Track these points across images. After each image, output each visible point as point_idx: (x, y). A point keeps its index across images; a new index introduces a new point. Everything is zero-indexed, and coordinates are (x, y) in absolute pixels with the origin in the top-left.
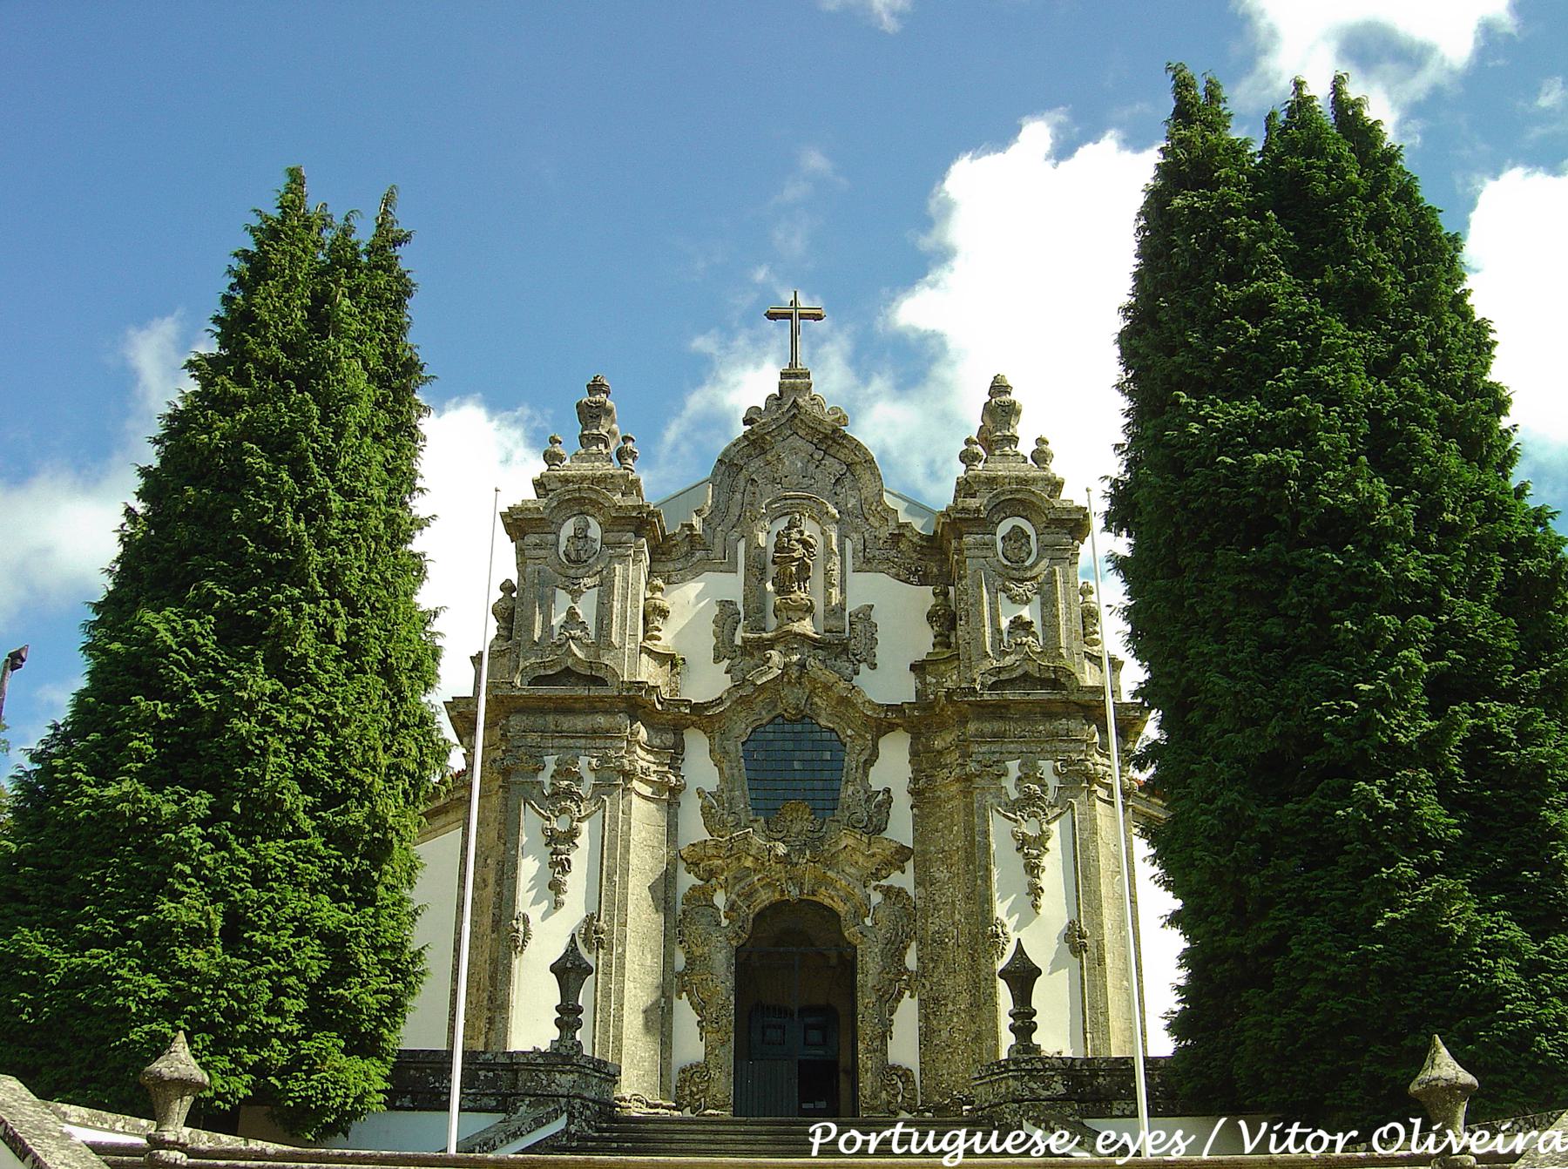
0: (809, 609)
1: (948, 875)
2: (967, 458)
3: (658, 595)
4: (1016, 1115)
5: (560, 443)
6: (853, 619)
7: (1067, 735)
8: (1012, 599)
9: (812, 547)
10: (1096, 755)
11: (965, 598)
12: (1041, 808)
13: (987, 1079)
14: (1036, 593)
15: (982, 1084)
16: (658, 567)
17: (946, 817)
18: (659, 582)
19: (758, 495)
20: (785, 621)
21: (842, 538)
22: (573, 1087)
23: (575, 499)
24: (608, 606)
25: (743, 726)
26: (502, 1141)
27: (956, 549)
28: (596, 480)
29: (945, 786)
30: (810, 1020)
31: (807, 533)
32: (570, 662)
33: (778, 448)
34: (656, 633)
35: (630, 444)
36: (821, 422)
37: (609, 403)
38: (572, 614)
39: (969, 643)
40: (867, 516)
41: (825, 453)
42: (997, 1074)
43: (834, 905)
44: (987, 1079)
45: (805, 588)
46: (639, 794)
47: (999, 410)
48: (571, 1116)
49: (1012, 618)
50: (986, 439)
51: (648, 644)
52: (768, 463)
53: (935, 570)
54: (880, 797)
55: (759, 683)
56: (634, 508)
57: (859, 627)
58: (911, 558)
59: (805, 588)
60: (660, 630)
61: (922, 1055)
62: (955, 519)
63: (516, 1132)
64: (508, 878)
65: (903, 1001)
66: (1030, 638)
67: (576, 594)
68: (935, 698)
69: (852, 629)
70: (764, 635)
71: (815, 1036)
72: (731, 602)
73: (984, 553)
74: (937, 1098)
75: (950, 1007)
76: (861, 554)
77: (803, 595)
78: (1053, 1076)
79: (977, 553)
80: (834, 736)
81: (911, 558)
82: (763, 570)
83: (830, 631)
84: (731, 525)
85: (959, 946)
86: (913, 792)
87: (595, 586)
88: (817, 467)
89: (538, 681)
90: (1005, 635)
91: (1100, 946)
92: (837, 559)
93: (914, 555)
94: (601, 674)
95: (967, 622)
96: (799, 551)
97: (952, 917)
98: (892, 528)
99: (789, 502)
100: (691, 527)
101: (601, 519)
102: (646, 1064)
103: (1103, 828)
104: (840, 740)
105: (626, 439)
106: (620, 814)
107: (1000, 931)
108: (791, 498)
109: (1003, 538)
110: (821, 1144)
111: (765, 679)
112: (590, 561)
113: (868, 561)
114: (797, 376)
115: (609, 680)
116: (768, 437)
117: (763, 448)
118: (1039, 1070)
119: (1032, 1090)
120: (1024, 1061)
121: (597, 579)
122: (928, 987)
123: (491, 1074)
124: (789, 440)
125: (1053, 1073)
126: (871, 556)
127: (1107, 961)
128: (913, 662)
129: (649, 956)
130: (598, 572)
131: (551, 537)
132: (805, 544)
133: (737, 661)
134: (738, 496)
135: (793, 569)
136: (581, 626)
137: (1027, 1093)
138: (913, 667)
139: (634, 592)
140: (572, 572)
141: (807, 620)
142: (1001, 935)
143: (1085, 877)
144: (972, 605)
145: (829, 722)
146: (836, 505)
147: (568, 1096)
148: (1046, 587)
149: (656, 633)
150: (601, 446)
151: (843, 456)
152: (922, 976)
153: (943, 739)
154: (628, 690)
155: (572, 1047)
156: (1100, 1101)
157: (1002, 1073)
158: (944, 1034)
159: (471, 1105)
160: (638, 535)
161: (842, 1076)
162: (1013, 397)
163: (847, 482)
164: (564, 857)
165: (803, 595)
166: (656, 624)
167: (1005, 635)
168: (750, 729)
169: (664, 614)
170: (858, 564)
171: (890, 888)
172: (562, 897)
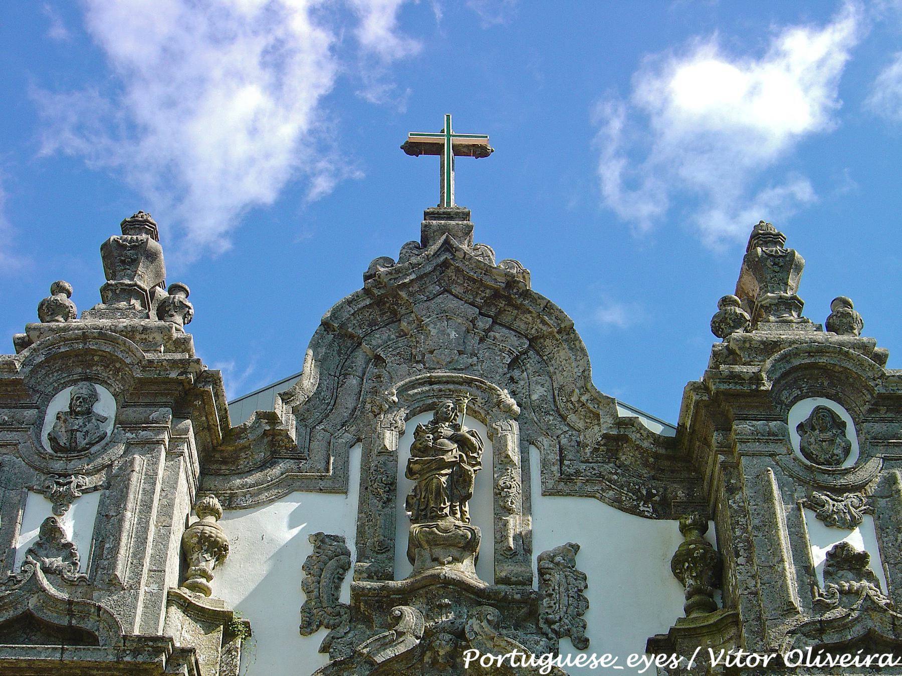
0: (469, 546)
3: (211, 519)
6: (546, 564)
8: (827, 520)
9: (473, 449)
11: (742, 521)
14: (865, 512)
16: (213, 482)
18: (215, 502)
19: (385, 379)
20: (429, 562)
21: (526, 442)
23: (77, 354)
24: (114, 520)
27: (721, 445)
31: (465, 429)
32: (32, 603)
33: (419, 309)
35: (181, 296)
38: (50, 531)
39: (756, 594)
41: (494, 322)
45: (462, 512)
47: (769, 263)
49: (829, 548)
52: (402, 334)
53: (680, 493)
55: (379, 659)
57: (556, 577)
58: (640, 476)
59: (462, 512)
62: (718, 393)
66: (864, 583)
67: (61, 502)
69: (544, 582)
70: (391, 583)
72: (335, 538)
73: (771, 448)
76: (555, 468)
79: (756, 447)
81: (640, 476)
82: (391, 486)
83: (506, 581)
84: (338, 421)
87: (96, 489)
88: (482, 340)
90: (820, 578)
92: (517, 473)
93: (644, 472)
94: (88, 625)
95: (749, 560)
96: (453, 453)
98: (606, 425)
99: (436, 387)
100: (272, 418)
101: (118, 387)
108: (439, 381)
109: (800, 427)
110: (470, 661)
111: (389, 653)
112: (93, 449)
113: (567, 478)
114: (449, 216)
115: (101, 635)
116: (403, 294)
117: (394, 313)
121: (99, 479)
124: (438, 300)
126: (572, 471)
128: (652, 636)
130: (104, 467)
131: (30, 413)
133: (341, 631)
134: (353, 381)
135: (443, 479)
136: (65, 553)
140: (58, 466)
141: (465, 562)
144: (756, 528)
146: (513, 394)
148: (882, 502)
151: (523, 326)
154: (136, 652)
160: (179, 415)
162: (788, 246)
163: (532, 361)
166: (203, 564)
167: (820, 578)
169: (218, 550)
170: (550, 484)
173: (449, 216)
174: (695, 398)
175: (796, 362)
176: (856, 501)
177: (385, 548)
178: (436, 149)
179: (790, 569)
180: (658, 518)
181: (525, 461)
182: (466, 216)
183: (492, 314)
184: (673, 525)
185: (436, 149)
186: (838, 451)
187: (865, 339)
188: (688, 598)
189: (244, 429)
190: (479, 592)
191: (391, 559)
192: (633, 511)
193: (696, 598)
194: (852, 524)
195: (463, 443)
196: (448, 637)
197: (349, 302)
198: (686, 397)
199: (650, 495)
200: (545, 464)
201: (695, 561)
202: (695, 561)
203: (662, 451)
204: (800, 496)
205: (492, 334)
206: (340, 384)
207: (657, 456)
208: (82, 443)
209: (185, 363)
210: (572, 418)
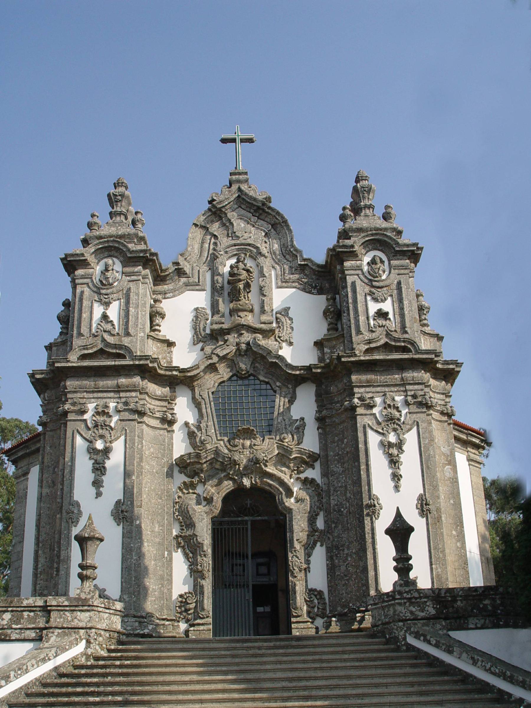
1: (342, 469)
2: (343, 218)
4: (401, 630)
5: (98, 217)
7: (413, 380)
8: (376, 300)
9: (251, 273)
10: (431, 393)
12: (399, 425)
13: (379, 605)
15: (376, 608)
17: (340, 434)
22: (89, 621)
25: (213, 382)
26: (33, 666)
28: (122, 237)
29: (338, 414)
30: (261, 560)
31: (248, 265)
34: (157, 327)
36: (255, 199)
37: (127, 193)
38: (105, 317)
40: (285, 255)
42: (387, 601)
43: (273, 491)
44: (379, 605)
45: (248, 297)
46: (148, 425)
48: (88, 642)
50: (354, 209)
51: (152, 334)
53: (327, 285)
54: (298, 423)
56: (141, 251)
59: (248, 297)
60: (160, 326)
61: (329, 582)
63: (45, 658)
64: (67, 480)
65: (316, 548)
67: (107, 304)
68: (330, 361)
71: (263, 570)
74: (339, 609)
75: (346, 551)
77: (247, 302)
78: (426, 602)
80: (268, 387)
85: (350, 513)
86: (318, 419)
89: (84, 357)
91: (438, 510)
97: (345, 495)
101: (122, 259)
102: (156, 593)
103: (437, 437)
104: (272, 389)
105: (136, 213)
106: (136, 438)
107: (376, 503)
114: (240, 174)
118: (416, 598)
119: (412, 613)
120: (406, 592)
122: (331, 539)
123: (32, 614)
125: (426, 600)
127: (443, 519)
128: (315, 340)
129: (157, 526)
132: (248, 271)
137: (408, 615)
138: (316, 344)
139: (143, 302)
140: (103, 291)
142: (377, 505)
143: (428, 467)
145: (266, 377)
147: (86, 628)
149: (157, 327)
150: (123, 218)
152: (328, 532)
153: (336, 386)
155: (89, 593)
156: (460, 618)
157: (390, 601)
158: (343, 568)
159: (18, 636)
161: (280, 594)
164: (101, 465)
165: (247, 302)
168: (217, 384)
171: (306, 479)
172: (101, 489)
173: (240, 174)
174: (331, 253)
176: (386, 292)
178: (234, 140)
180: (319, 294)
182: (246, 173)
183: (257, 215)
184: (324, 297)
185: (234, 140)
187: (395, 226)
188: (329, 325)
192: (310, 292)
193: (331, 326)
194: (384, 300)
195: (248, 271)
196: (245, 345)
198: (328, 253)
199: (316, 286)
200: (277, 276)
201: (331, 312)
202: (331, 312)
203: (320, 270)
204: (367, 289)
205: (257, 223)
209: (145, 251)
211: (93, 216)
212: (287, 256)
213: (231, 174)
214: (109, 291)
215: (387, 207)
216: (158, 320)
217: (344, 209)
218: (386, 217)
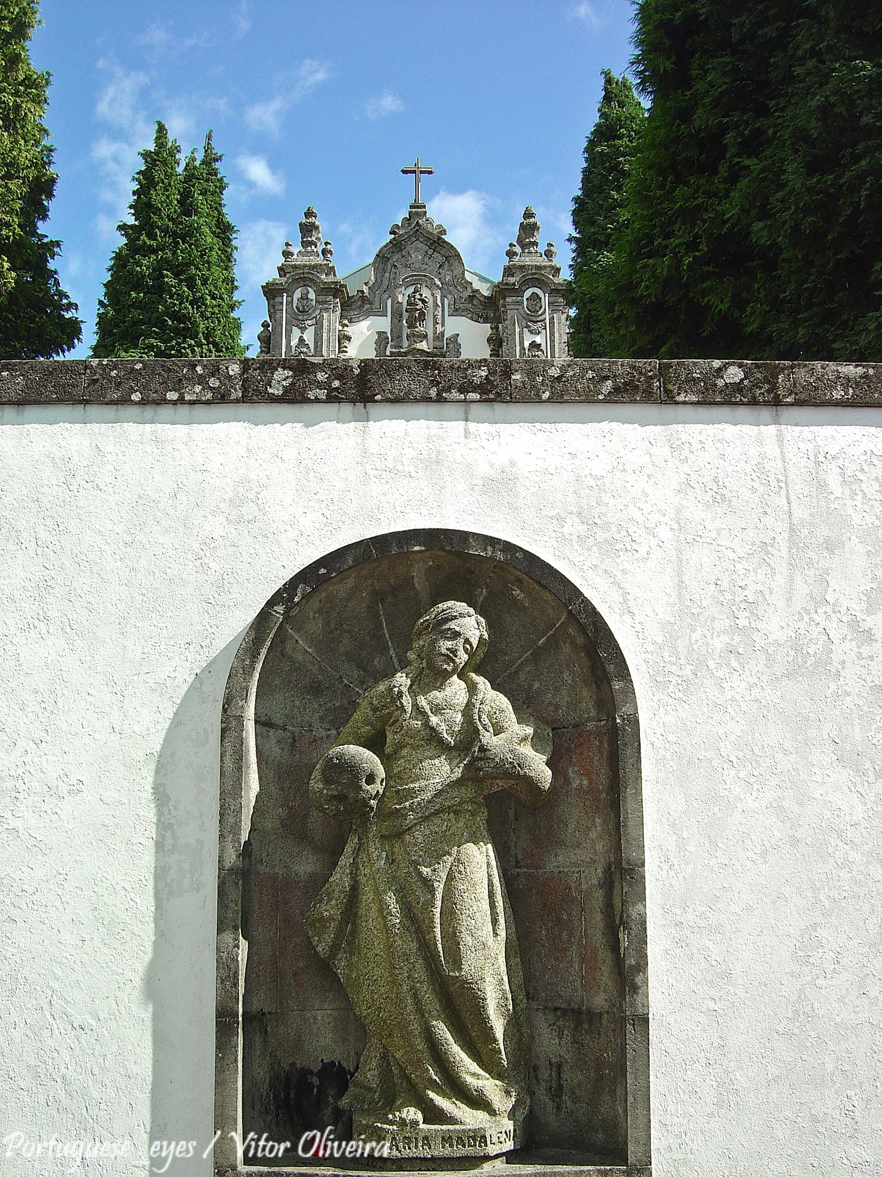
0: (425, 336)
6: (448, 341)
8: (531, 332)
9: (427, 303)
31: (424, 295)
34: (345, 349)
35: (329, 246)
38: (301, 340)
49: (530, 342)
57: (451, 346)
67: (303, 329)
69: (447, 347)
72: (384, 332)
73: (517, 307)
77: (422, 329)
79: (514, 307)
82: (401, 315)
92: (440, 309)
93: (481, 307)
98: (469, 292)
100: (362, 292)
105: (327, 243)
109: (527, 299)
113: (456, 310)
114: (418, 207)
121: (314, 321)
132: (423, 301)
140: (301, 318)
149: (345, 349)
160: (335, 298)
165: (422, 329)
169: (349, 339)
170: (451, 312)
175: (527, 278)
177: (400, 337)
179: (518, 348)
181: (443, 304)
186: (538, 308)
189: (353, 296)
190: (428, 353)
191: (402, 340)
195: (423, 301)
197: (385, 247)
206: (383, 276)
207: (485, 302)
208: (307, 310)
210: (458, 287)
211: (287, 244)
212: (458, 287)
213: (411, 207)
214: (305, 317)
215: (550, 245)
216: (346, 343)
217: (511, 245)
218: (549, 254)
